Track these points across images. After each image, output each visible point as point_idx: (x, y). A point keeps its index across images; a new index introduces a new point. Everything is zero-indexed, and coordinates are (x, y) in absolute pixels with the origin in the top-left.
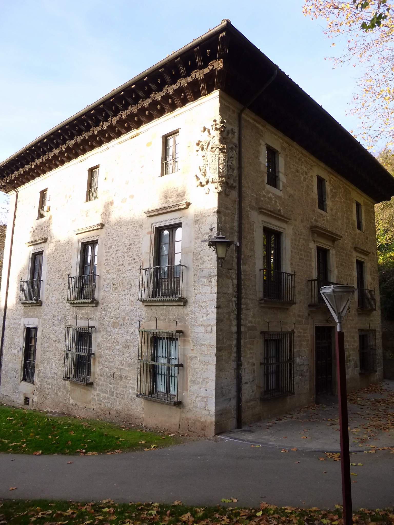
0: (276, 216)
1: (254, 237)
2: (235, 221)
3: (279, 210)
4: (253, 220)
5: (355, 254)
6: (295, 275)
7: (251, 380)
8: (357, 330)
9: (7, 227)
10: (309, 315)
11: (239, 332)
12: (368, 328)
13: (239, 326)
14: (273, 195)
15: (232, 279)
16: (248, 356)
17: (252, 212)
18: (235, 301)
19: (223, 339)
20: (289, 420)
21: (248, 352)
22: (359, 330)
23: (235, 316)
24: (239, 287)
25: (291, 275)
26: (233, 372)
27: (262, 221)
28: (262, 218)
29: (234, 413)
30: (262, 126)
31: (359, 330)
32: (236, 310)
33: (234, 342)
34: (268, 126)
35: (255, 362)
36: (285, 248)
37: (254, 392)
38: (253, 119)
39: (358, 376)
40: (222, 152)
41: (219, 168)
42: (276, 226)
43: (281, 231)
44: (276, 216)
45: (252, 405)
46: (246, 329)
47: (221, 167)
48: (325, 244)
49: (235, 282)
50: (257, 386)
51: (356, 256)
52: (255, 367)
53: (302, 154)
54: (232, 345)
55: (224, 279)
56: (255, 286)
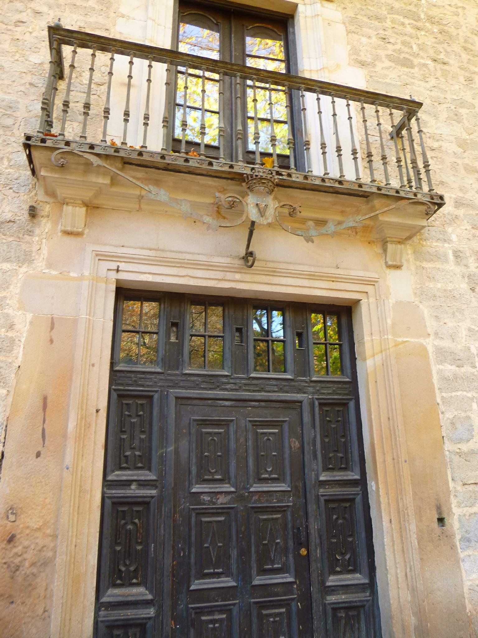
10: (33, 213)
47: (151, 366)
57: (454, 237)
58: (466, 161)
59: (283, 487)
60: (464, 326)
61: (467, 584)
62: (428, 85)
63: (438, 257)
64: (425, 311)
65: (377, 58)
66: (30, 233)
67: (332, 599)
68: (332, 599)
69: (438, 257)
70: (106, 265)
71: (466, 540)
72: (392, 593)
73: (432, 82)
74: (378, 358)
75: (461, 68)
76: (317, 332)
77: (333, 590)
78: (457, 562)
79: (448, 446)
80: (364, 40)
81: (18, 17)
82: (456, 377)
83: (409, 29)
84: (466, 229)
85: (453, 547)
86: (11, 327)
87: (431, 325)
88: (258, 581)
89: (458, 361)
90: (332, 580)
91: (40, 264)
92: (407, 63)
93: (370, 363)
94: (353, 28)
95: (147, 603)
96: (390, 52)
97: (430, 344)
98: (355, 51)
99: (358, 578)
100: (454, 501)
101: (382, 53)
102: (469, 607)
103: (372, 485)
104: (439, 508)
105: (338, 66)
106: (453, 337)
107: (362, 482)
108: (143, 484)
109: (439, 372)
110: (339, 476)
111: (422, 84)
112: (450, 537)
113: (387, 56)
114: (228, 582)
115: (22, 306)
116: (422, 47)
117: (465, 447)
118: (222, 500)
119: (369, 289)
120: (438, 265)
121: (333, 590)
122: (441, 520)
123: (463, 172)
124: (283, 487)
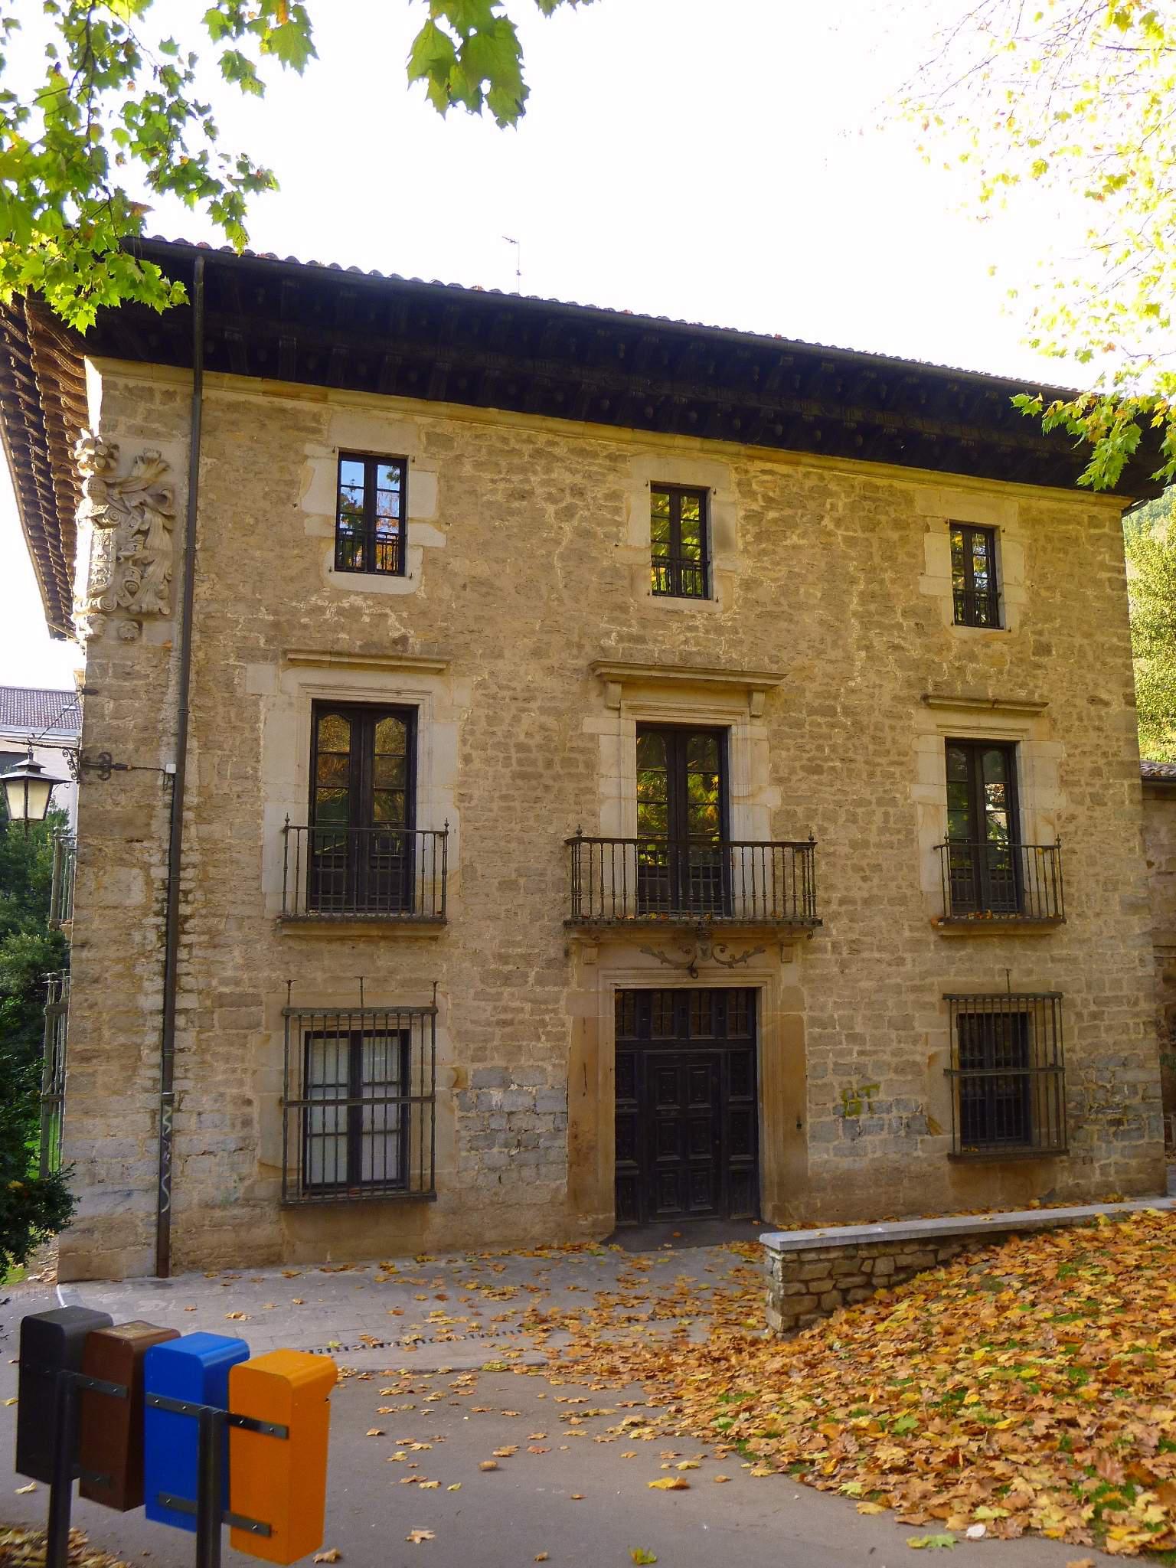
0: (372, 662)
1: (257, 740)
2: (165, 706)
3: (403, 640)
4: (250, 691)
5: (923, 719)
6: (1059, 847)
7: (233, 1146)
8: (935, 998)
9: (48, 634)
10: (567, 953)
11: (169, 1011)
12: (1003, 988)
13: (170, 991)
14: (366, 599)
15: (146, 867)
16: (220, 1078)
17: (251, 667)
18: (158, 927)
19: (98, 1029)
20: (417, 1266)
21: (221, 1066)
22: (945, 997)
23: (158, 968)
24: (172, 890)
25: (1052, 848)
26: (144, 1120)
27: (303, 685)
28: (294, 679)
29: (147, 1232)
30: (316, 400)
31: (945, 997)
32: (163, 949)
33: (153, 1038)
34: (335, 395)
35: (249, 1094)
36: (430, 753)
37: (247, 1183)
38: (265, 393)
39: (946, 1166)
40: (102, 526)
41: (91, 570)
42: (372, 689)
43: (415, 702)
44: (372, 662)
45: (234, 1217)
46: (208, 1003)
47: (95, 569)
48: (694, 711)
49: (161, 873)
50: (262, 1164)
51: (939, 726)
52: (254, 1111)
53: (550, 431)
54: (138, 1047)
55: (108, 868)
56: (258, 877)
57: (834, 932)
58: (855, 861)
59: (706, 1105)
60: (831, 1001)
61: (811, 1161)
62: (833, 790)
63: (823, 950)
64: (805, 991)
65: (793, 771)
66: (566, 965)
67: (733, 1167)
68: (733, 1167)
69: (823, 950)
70: (609, 981)
71: (813, 1137)
72: (766, 1165)
73: (838, 785)
74: (770, 1027)
75: (866, 762)
76: (707, 822)
77: (732, 1163)
78: (806, 1148)
79: (809, 1081)
80: (784, 754)
81: (535, 794)
82: (821, 1036)
83: (825, 730)
84: (1087, 356)
85: (805, 1141)
86: (563, 1025)
87: (808, 1001)
88: (692, 1157)
89: (823, 1025)
90: (733, 1158)
91: (574, 985)
92: (818, 770)
93: (764, 1030)
94: (775, 743)
95: (634, 1168)
96: (804, 762)
97: (805, 1015)
98: (776, 769)
99: (748, 1157)
100: (808, 1115)
101: (797, 764)
102: (810, 1173)
103: (760, 1105)
104: (799, 1119)
105: (760, 788)
106: (822, 1008)
107: (755, 1103)
108: (630, 1106)
109: (810, 1033)
110: (740, 1098)
111: (828, 789)
112: (803, 1135)
113: (802, 767)
114: (676, 1158)
115: (568, 1013)
116: (833, 749)
117: (820, 1082)
118: (673, 1113)
119: (768, 979)
120: (819, 956)
121: (732, 1163)
122: (799, 1126)
123: (850, 872)
124: (706, 1105)
